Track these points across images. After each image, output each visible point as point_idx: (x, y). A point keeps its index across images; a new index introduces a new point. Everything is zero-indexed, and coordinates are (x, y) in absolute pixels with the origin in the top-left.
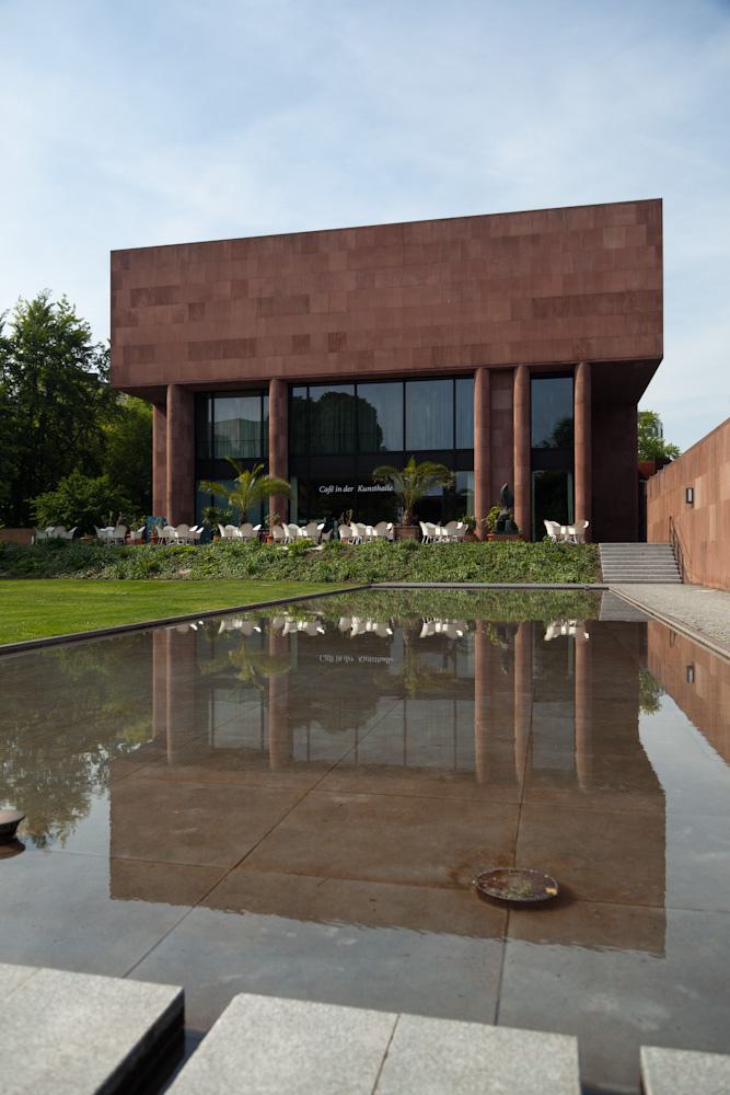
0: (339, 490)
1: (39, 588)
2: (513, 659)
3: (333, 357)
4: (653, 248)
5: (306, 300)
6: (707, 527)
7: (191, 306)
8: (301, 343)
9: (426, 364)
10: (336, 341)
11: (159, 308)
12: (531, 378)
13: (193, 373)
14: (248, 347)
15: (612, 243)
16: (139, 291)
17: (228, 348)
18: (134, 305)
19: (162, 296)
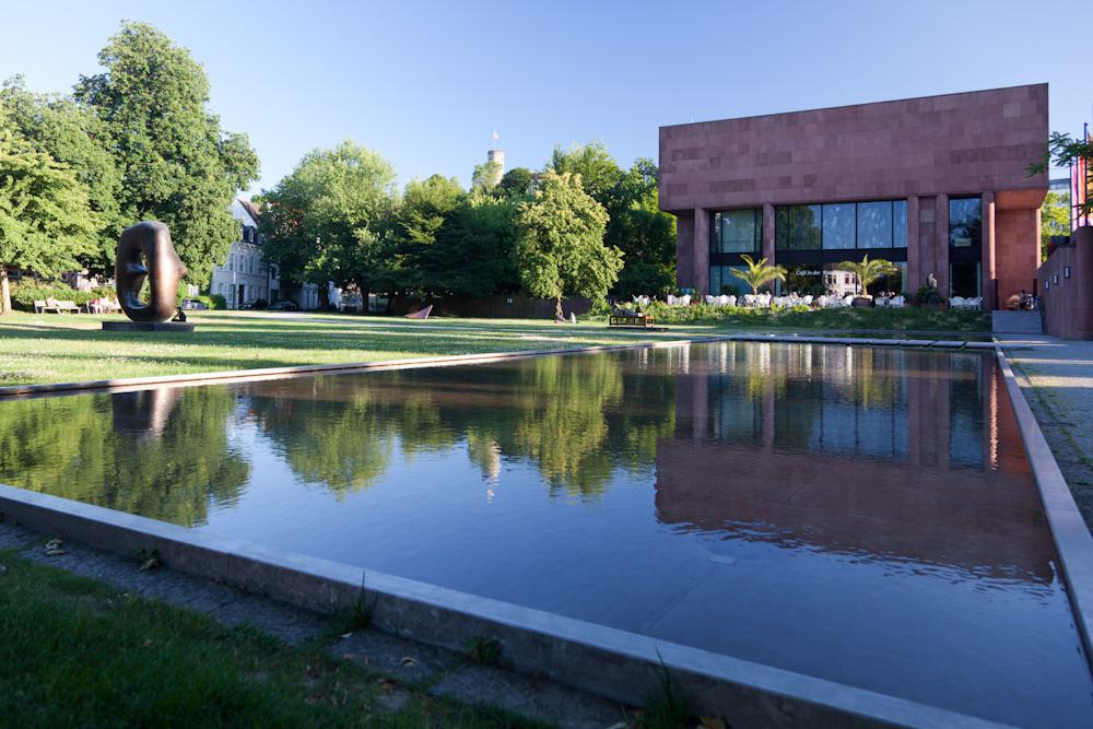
0: (810, 273)
1: (50, 373)
2: (690, 355)
3: (807, 190)
4: (1041, 116)
5: (790, 155)
6: (230, 333)
7: (711, 160)
8: (786, 182)
9: (873, 194)
10: (809, 181)
11: (690, 162)
12: (711, 265)
13: (713, 200)
14: (750, 184)
15: (1010, 112)
16: (677, 151)
17: (735, 186)
18: (674, 160)
19: (692, 154)
